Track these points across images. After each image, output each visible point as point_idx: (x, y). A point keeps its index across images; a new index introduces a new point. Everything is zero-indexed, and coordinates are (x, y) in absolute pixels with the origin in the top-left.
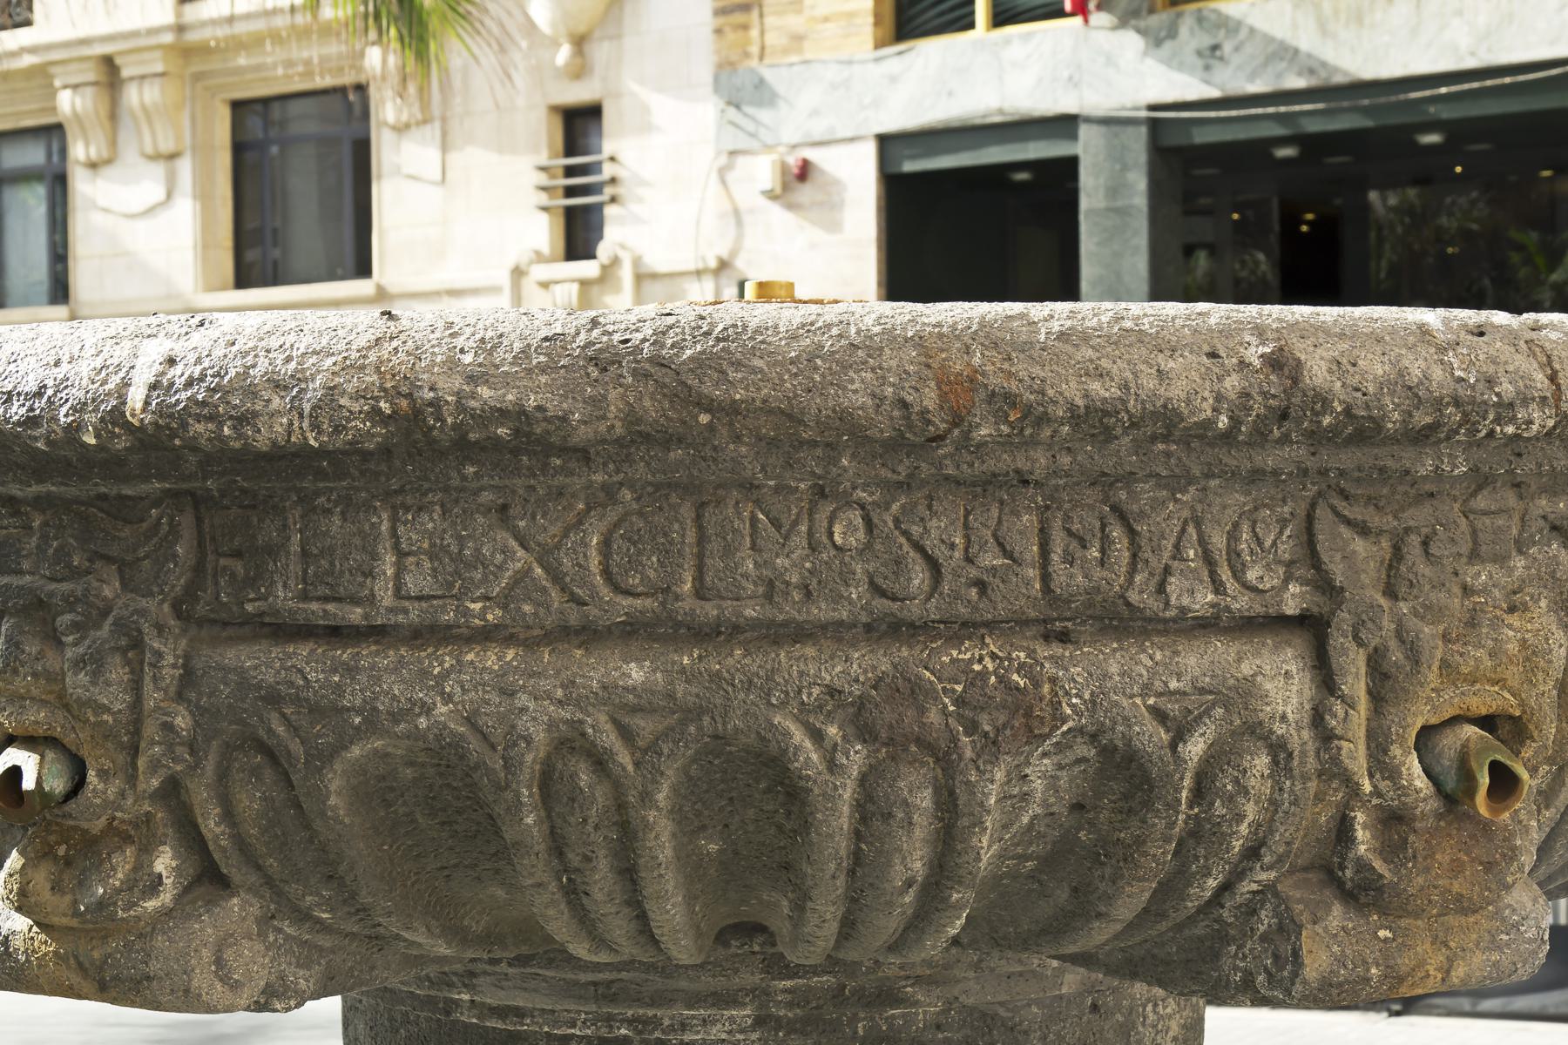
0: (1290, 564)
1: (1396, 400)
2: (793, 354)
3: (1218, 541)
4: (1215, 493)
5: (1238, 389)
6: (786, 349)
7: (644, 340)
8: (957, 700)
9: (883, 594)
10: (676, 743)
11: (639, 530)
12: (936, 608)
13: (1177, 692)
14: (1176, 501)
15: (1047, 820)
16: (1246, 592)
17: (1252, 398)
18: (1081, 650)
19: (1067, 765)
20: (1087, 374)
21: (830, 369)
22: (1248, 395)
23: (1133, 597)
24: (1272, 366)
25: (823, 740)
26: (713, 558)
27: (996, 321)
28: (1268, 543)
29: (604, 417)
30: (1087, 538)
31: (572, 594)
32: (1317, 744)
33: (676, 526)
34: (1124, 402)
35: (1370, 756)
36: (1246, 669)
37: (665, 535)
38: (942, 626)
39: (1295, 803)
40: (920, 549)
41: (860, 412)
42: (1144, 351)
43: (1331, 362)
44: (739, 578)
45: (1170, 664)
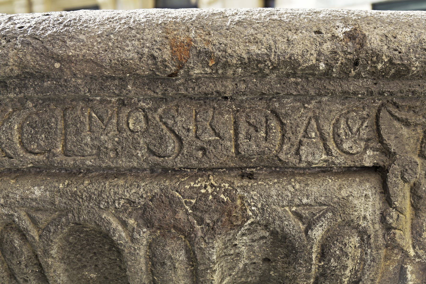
0: (368, 140)
1: (417, 56)
2: (100, 32)
3: (328, 129)
4: (326, 104)
5: (330, 49)
6: (97, 30)
7: (30, 26)
8: (192, 207)
9: (154, 154)
10: (57, 226)
11: (36, 122)
12: (180, 161)
13: (306, 205)
14: (305, 108)
15: (253, 266)
16: (344, 154)
17: (338, 54)
18: (257, 183)
19: (256, 240)
20: (249, 42)
21: (117, 39)
22: (336, 52)
23: (282, 156)
24: (350, 38)
25: (127, 226)
26: (71, 136)
27: (206, 15)
28: (355, 130)
29: (6, 65)
30: (258, 126)
31: (6, 153)
32: (384, 231)
33: (53, 120)
34: (268, 56)
35: (413, 238)
36: (344, 193)
37: (48, 124)
38: (189, 170)
39: (373, 260)
40: (173, 131)
41: (131, 61)
42: (281, 30)
43: (382, 36)
44: (83, 145)
45: (303, 190)
